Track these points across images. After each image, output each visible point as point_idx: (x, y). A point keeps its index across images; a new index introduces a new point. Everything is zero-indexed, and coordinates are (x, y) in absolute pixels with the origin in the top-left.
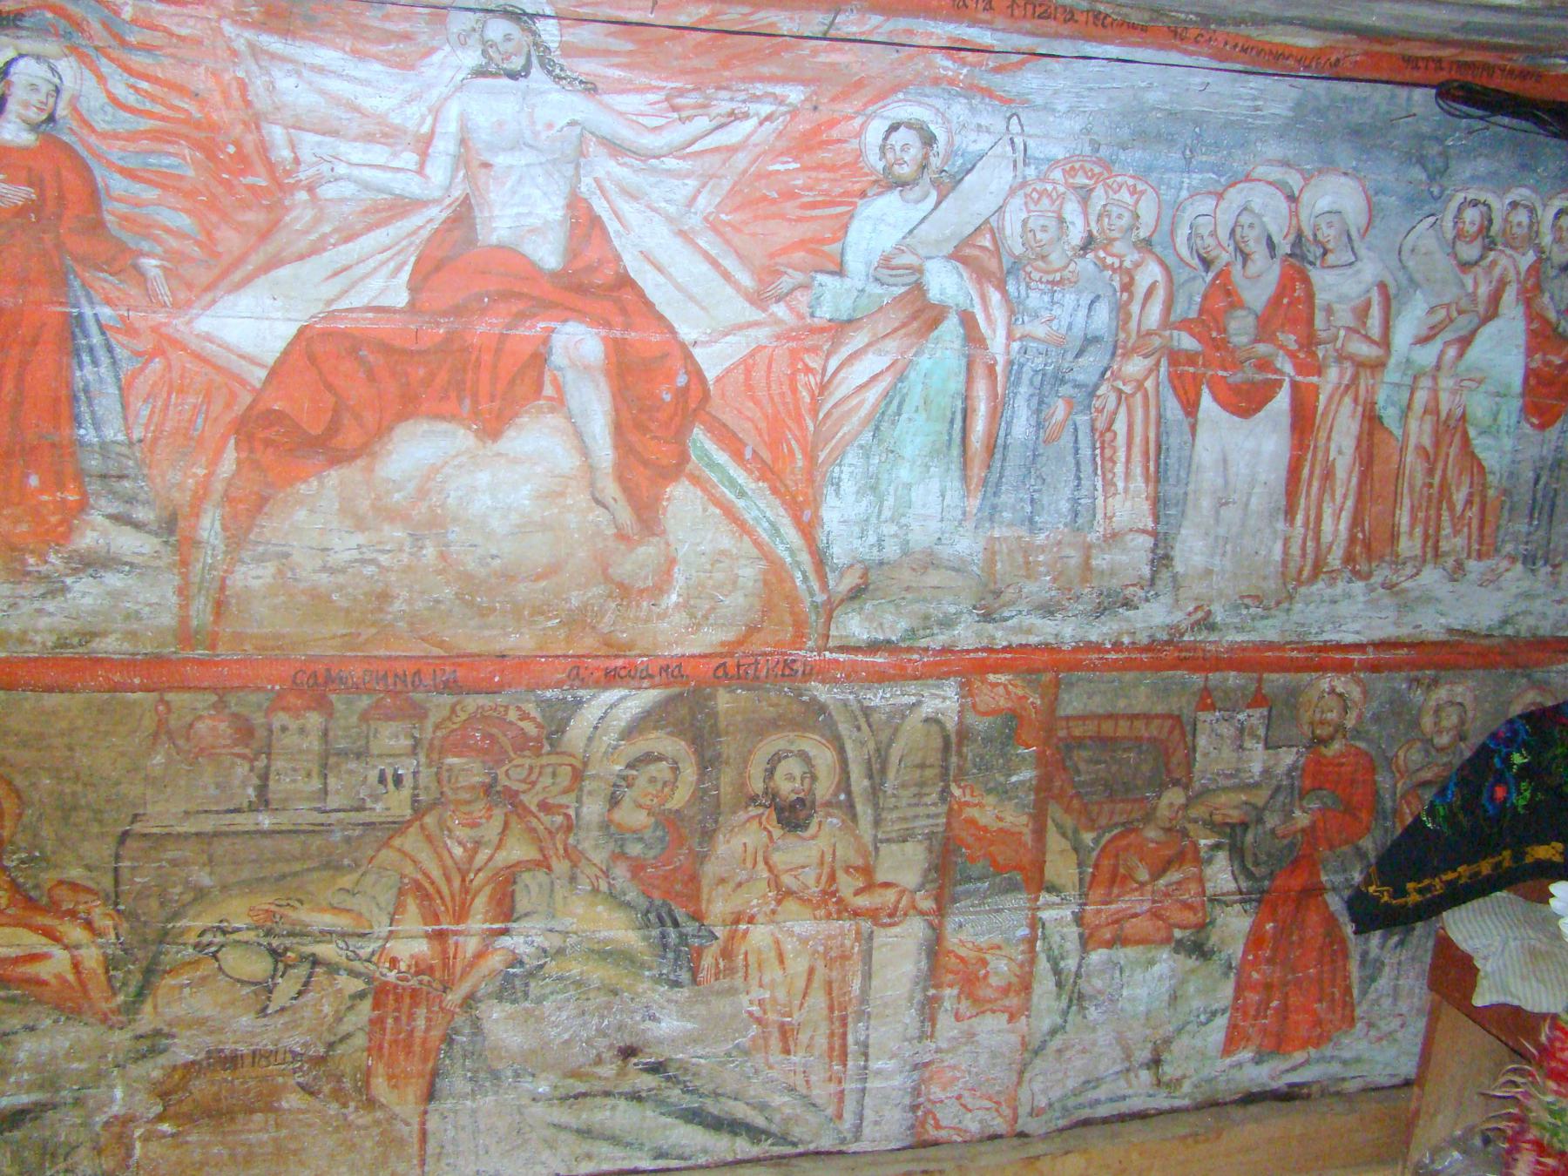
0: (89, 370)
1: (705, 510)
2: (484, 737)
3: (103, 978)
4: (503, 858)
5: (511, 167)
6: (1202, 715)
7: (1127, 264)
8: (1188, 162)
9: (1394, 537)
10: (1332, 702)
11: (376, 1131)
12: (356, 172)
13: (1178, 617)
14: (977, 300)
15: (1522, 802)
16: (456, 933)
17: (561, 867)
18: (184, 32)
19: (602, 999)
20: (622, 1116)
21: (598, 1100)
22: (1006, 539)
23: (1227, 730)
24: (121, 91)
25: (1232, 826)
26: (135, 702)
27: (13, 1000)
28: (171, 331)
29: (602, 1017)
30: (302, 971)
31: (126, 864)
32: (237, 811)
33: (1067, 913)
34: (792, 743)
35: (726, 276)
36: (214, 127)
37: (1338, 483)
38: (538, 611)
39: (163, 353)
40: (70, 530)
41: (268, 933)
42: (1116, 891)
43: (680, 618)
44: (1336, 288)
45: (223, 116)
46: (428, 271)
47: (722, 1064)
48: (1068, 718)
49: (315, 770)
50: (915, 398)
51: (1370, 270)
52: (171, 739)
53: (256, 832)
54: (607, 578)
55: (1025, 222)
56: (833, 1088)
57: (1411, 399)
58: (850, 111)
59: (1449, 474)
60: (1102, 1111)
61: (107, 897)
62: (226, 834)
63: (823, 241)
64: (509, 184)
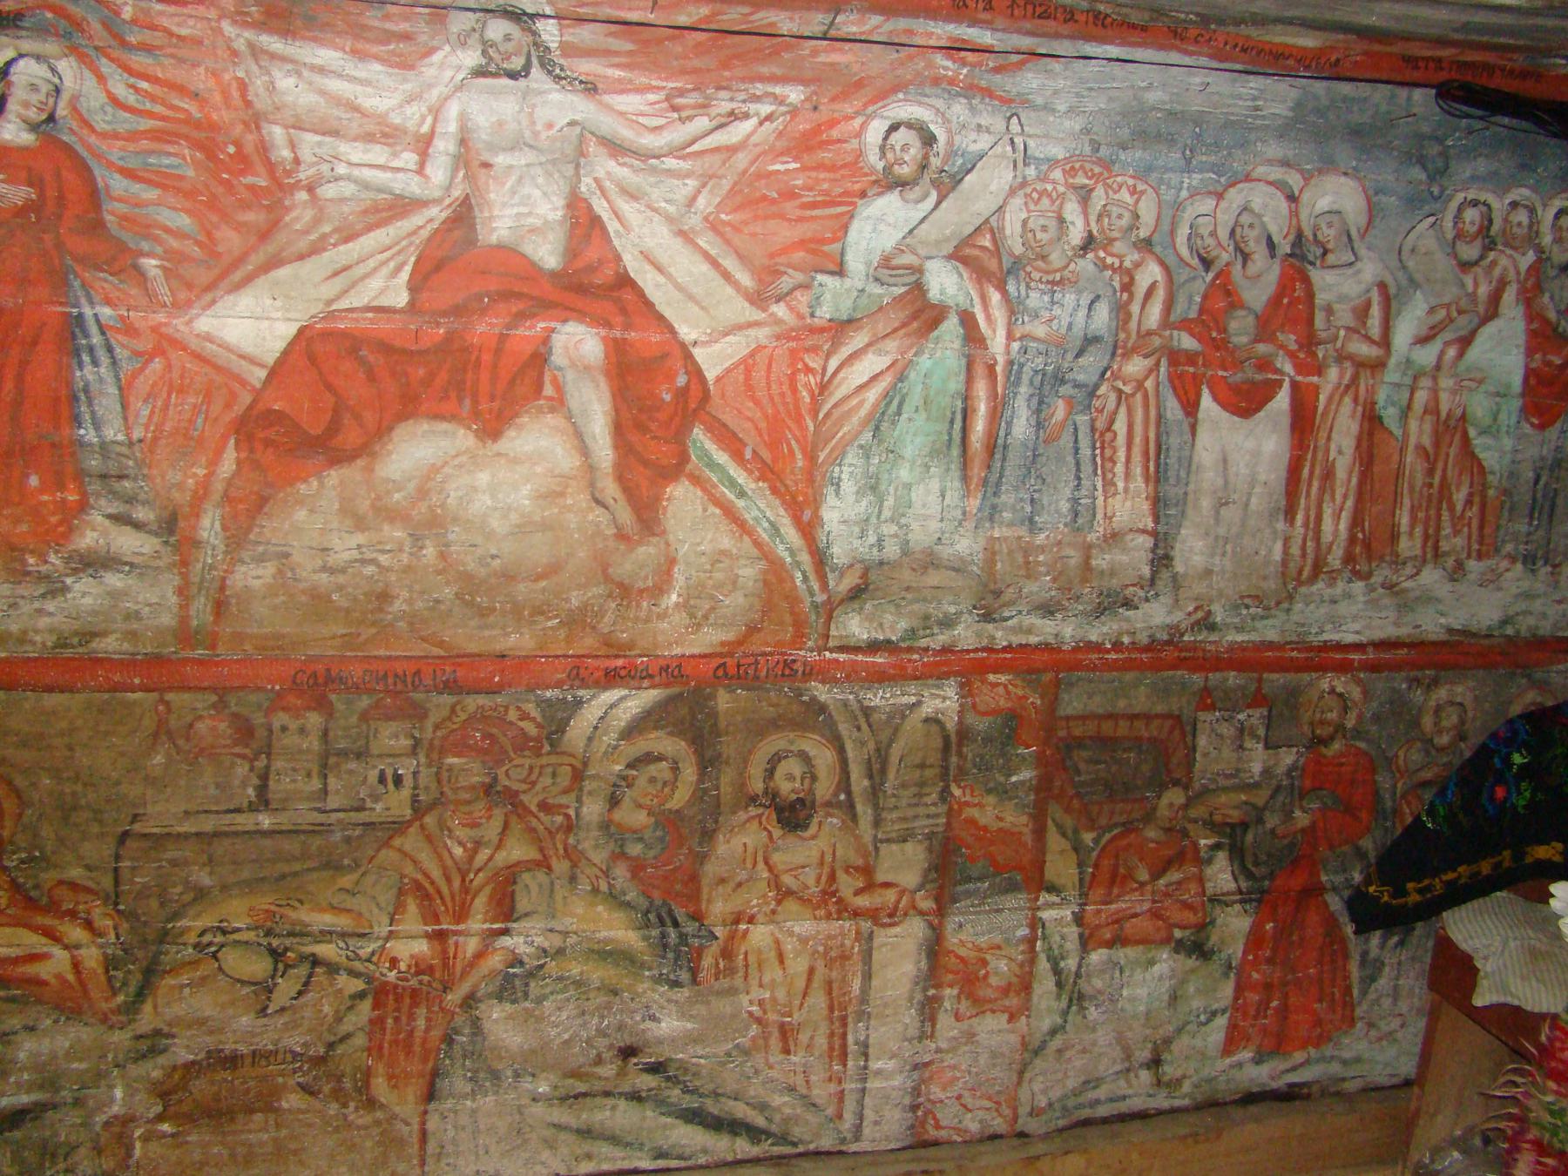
0: (88, 368)
1: (705, 510)
2: (484, 738)
3: (103, 978)
4: (502, 858)
5: (511, 167)
6: (1202, 716)
7: (1127, 264)
8: (1188, 161)
9: (1394, 537)
10: (1331, 701)
11: (376, 1131)
12: (356, 172)
13: (1178, 616)
14: (977, 300)
15: (1522, 802)
16: (456, 933)
17: (561, 866)
18: (184, 32)
19: (602, 999)
20: (622, 1116)
21: (599, 1100)
22: (1006, 539)
23: (1227, 730)
24: (121, 91)
25: (1232, 826)
26: (135, 702)
27: (12, 1000)
29: (602, 1017)
30: (302, 971)
32: (238, 811)
33: (1067, 913)
34: (791, 742)
35: (727, 276)
36: (213, 127)
37: (1338, 483)
38: (538, 611)
40: (71, 530)
41: (268, 933)
42: (1116, 891)
43: (680, 618)
44: (1336, 287)
45: (222, 116)
46: (427, 272)
47: (723, 1064)
48: (1068, 718)
49: (315, 770)
50: (915, 399)
51: (1370, 270)
53: (256, 832)
54: (607, 578)
55: (1025, 222)
56: (833, 1088)
57: (1411, 399)
59: (1449, 473)
60: (1102, 1111)
62: (226, 834)
63: (823, 241)
64: (509, 185)
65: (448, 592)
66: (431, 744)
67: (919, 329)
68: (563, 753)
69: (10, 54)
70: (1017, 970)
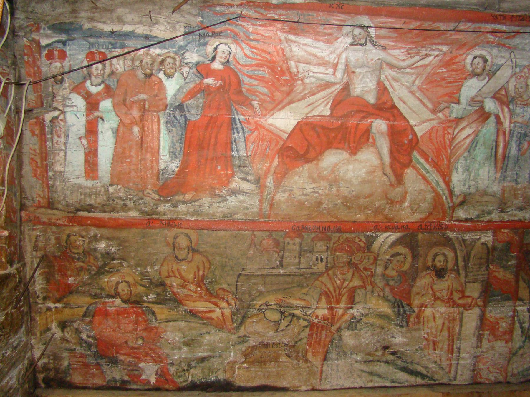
0: (236, 134)
1: (417, 177)
3: (230, 318)
4: (351, 285)
5: (360, 73)
11: (307, 369)
12: (315, 75)
14: (500, 111)
16: (337, 308)
17: (369, 288)
18: (266, 35)
19: (379, 330)
20: (381, 368)
22: (508, 186)
24: (248, 52)
27: (204, 324)
28: (260, 123)
29: (379, 336)
30: (289, 318)
31: (239, 284)
33: (525, 308)
34: (441, 250)
35: (424, 105)
36: (274, 62)
39: (258, 130)
40: (229, 182)
41: (280, 306)
45: (277, 59)
47: (415, 353)
48: (527, 244)
49: (297, 256)
50: (481, 141)
52: (255, 245)
53: (278, 275)
54: (387, 198)
55: (515, 86)
56: (448, 362)
58: (462, 53)
61: (234, 293)
62: (270, 275)
63: (454, 93)
64: (360, 78)
65: (339, 202)
66: (332, 249)
67: (482, 120)
68: (371, 252)
69: (218, 43)
70: (509, 327)
